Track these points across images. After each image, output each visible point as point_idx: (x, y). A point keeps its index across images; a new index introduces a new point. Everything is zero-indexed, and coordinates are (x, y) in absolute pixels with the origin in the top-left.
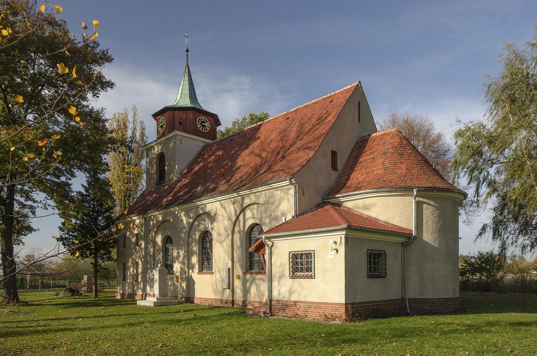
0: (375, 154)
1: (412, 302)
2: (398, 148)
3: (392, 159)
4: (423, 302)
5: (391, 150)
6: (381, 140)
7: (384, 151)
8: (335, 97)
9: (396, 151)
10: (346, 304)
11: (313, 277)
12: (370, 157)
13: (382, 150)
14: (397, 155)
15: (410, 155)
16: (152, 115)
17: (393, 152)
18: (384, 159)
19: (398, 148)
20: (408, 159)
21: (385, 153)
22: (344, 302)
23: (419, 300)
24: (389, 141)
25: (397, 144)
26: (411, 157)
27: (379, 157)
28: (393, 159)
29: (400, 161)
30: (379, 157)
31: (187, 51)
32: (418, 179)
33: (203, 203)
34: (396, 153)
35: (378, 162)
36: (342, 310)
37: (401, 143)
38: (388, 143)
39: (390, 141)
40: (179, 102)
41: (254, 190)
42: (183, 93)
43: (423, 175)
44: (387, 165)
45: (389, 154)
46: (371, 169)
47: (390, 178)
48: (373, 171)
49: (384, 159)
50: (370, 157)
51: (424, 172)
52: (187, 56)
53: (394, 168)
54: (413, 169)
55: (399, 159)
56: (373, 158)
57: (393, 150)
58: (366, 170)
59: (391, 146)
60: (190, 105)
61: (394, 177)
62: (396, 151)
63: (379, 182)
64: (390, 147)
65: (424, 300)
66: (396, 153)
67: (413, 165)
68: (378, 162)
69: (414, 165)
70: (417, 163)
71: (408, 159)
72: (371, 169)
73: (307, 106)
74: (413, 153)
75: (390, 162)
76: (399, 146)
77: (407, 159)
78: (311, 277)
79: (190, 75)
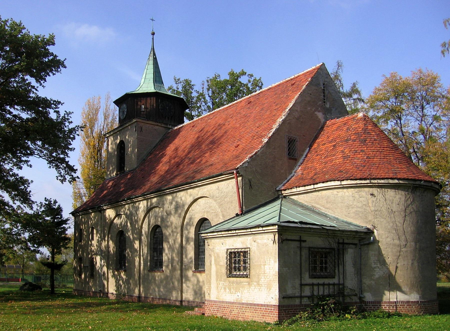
0: (337, 141)
1: (372, 306)
2: (361, 134)
3: (353, 147)
4: (385, 306)
5: (354, 136)
6: (346, 125)
7: (346, 138)
8: (298, 79)
9: (359, 138)
10: (279, 306)
11: (249, 276)
12: (332, 144)
13: (345, 137)
14: (359, 142)
15: (375, 142)
16: (114, 102)
17: (355, 138)
18: (345, 146)
19: (361, 134)
20: (371, 146)
21: (347, 141)
22: (278, 305)
23: (372, 303)
24: (353, 127)
25: (361, 129)
26: (374, 144)
27: (340, 144)
28: (355, 147)
29: (361, 149)
30: (340, 144)
31: (153, 34)
32: (378, 169)
33: (198, 185)
34: (359, 140)
35: (338, 151)
36: (275, 312)
37: (365, 130)
38: (351, 129)
39: (354, 126)
40: (143, 87)
41: (181, 187)
42: (146, 78)
43: (386, 164)
44: (346, 153)
45: (351, 141)
46: (330, 158)
47: (347, 168)
48: (331, 160)
49: (345, 146)
50: (332, 144)
51: (388, 160)
52: (153, 39)
53: (354, 156)
54: (376, 157)
55: (361, 146)
56: (334, 146)
57: (355, 136)
58: (326, 159)
59: (354, 132)
60: (154, 91)
61: (352, 167)
62: (359, 138)
63: (335, 172)
64: (353, 133)
65: (386, 304)
66: (359, 140)
67: (375, 153)
68: (338, 151)
69: (377, 153)
70: (381, 151)
71: (371, 146)
72: (330, 158)
73: (270, 89)
74: (378, 140)
75: (350, 150)
76: (363, 131)
77: (370, 146)
78: (247, 276)
79: (155, 59)
